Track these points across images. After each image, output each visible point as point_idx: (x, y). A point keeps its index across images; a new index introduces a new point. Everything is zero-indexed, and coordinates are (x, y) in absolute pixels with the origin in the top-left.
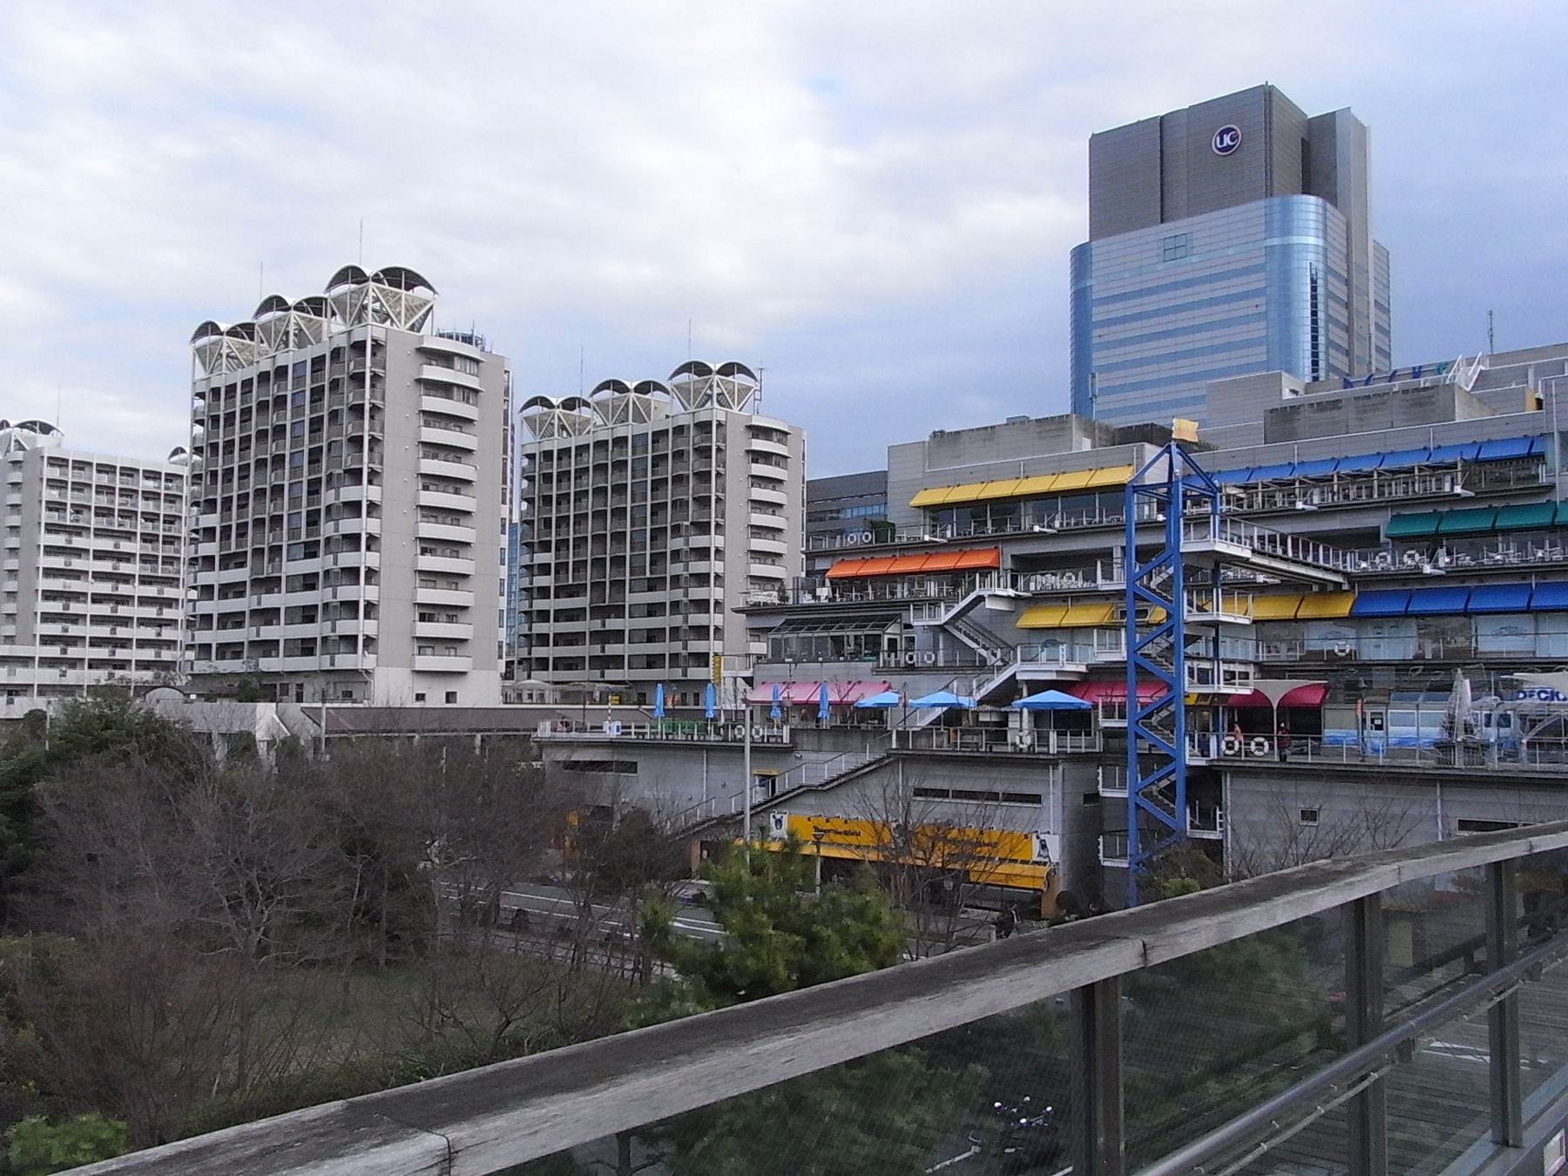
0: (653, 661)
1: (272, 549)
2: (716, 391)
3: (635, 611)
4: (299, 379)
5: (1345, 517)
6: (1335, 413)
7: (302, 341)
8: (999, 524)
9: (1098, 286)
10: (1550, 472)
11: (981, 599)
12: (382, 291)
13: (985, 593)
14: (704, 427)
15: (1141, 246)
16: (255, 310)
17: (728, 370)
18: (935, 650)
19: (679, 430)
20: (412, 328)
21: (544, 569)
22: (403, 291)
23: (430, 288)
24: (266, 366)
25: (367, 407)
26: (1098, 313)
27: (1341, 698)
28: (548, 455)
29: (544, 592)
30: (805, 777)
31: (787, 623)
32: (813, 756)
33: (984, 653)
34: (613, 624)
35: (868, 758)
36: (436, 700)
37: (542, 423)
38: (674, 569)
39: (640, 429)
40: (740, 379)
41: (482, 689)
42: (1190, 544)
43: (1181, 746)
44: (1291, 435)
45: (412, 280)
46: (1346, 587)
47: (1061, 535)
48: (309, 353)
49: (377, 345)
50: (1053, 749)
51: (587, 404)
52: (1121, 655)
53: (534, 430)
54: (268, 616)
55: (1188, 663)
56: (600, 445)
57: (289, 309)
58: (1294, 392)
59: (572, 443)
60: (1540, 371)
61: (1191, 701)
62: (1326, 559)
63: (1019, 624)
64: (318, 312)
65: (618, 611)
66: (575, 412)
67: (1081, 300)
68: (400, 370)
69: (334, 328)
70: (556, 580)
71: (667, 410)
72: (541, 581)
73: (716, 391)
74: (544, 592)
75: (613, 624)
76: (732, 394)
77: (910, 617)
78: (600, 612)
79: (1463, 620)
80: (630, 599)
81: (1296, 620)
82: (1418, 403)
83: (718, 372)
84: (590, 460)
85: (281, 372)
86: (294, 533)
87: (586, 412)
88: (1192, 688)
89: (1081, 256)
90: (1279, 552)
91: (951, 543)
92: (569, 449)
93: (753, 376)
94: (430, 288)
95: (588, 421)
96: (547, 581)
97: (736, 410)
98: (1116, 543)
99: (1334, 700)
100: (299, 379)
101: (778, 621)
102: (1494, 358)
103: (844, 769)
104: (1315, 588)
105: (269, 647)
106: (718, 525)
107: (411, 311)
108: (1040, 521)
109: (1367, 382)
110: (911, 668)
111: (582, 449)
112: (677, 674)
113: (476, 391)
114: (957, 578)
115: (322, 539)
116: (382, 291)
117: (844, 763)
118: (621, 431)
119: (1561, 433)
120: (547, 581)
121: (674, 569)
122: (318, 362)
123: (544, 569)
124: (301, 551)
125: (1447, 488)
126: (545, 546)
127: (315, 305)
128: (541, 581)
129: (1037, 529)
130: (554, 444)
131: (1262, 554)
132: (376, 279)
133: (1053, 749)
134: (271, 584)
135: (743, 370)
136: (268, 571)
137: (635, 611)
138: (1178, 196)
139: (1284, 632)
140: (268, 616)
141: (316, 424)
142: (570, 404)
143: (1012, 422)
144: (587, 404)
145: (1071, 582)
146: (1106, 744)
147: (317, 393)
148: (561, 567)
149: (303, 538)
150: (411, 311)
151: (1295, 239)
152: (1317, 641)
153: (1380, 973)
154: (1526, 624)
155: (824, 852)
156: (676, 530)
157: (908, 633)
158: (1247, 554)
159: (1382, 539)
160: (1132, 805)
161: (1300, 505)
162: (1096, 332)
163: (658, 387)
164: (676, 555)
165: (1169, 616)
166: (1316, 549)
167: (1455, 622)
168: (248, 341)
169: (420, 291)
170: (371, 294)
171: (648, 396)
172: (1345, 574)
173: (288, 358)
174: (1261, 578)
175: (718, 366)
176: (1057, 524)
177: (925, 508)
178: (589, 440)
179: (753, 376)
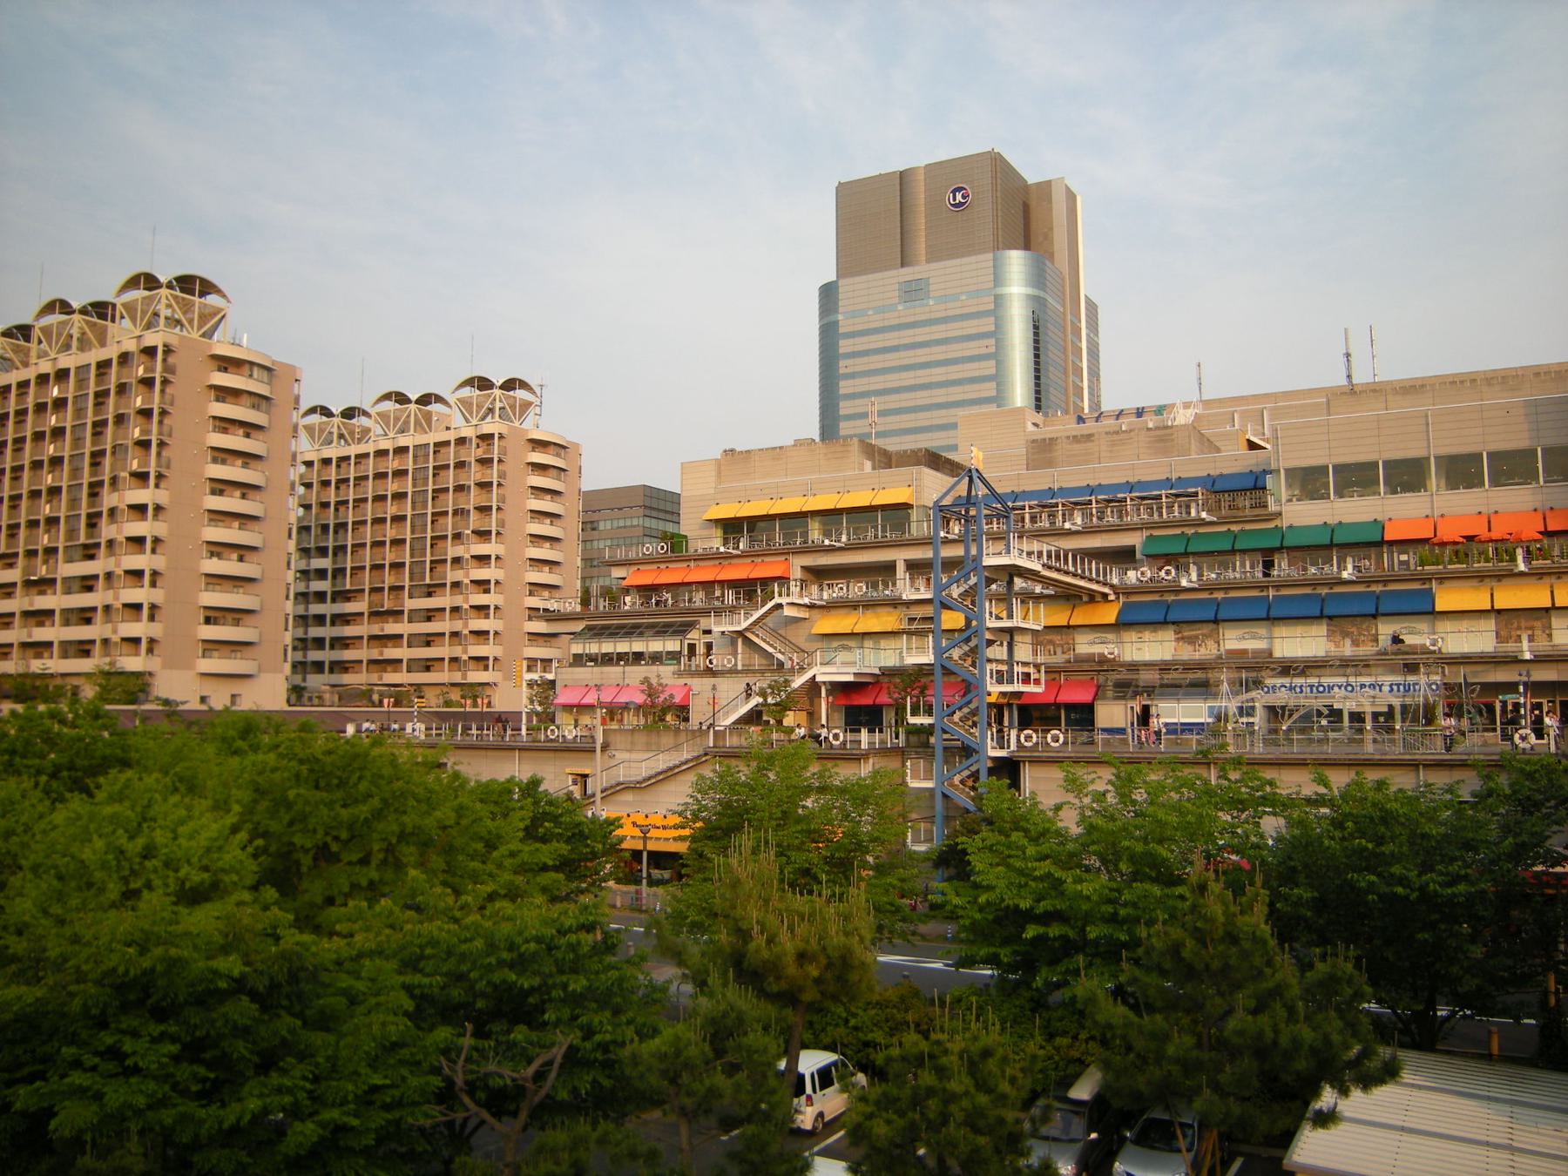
0: (428, 665)
1: (392, 588)
2: (498, 405)
3: (414, 616)
4: (82, 382)
5: (1104, 536)
6: (1089, 445)
7: (84, 345)
8: (789, 536)
9: (845, 323)
10: (1278, 501)
11: (780, 606)
12: (175, 297)
13: (784, 600)
14: (486, 438)
15: (877, 293)
16: (37, 309)
17: (510, 385)
18: (735, 654)
19: (461, 441)
20: (203, 335)
21: (321, 574)
22: (196, 299)
23: (224, 296)
24: (46, 367)
25: (156, 412)
26: (845, 346)
27: (1110, 694)
28: (326, 462)
29: (320, 597)
30: (622, 774)
31: (589, 628)
32: (626, 756)
33: (780, 657)
34: (391, 628)
35: (686, 756)
36: (219, 701)
37: (321, 431)
38: (452, 575)
39: (421, 439)
40: (520, 394)
41: (268, 693)
42: (993, 558)
43: (984, 737)
44: (1050, 464)
45: (207, 288)
46: (1112, 597)
47: (848, 548)
48: (94, 356)
49: (168, 350)
50: (864, 746)
51: (366, 414)
52: (928, 658)
53: (312, 437)
54: (41, 617)
55: (989, 667)
56: (381, 453)
57: (73, 312)
58: (1035, 425)
59: (353, 450)
60: (1243, 414)
61: (992, 699)
62: (1105, 574)
63: (814, 631)
64: (103, 316)
65: (396, 614)
66: (354, 421)
67: (829, 335)
68: (193, 377)
69: (124, 336)
70: (334, 585)
71: (455, 422)
72: (318, 586)
73: (498, 405)
74: (320, 597)
75: (391, 628)
76: (513, 407)
77: (704, 623)
78: (377, 615)
79: (1212, 626)
80: (410, 604)
81: (1068, 627)
82: (1161, 440)
83: (502, 387)
84: (370, 467)
85: (62, 375)
86: (72, 533)
87: (364, 421)
88: (995, 689)
89: (828, 294)
90: (1071, 569)
91: (743, 556)
92: (348, 458)
93: (534, 393)
94: (224, 296)
95: (369, 430)
96: (324, 586)
97: (517, 424)
98: (900, 556)
99: (1104, 698)
100: (82, 382)
101: (578, 626)
102: (1207, 404)
103: (662, 766)
104: (1085, 599)
105: (41, 648)
106: (498, 533)
107: (204, 318)
108: (827, 534)
109: (1097, 419)
110: (710, 672)
111: (362, 457)
112: (457, 677)
113: (267, 398)
114: (750, 590)
115: (103, 542)
116: (175, 297)
117: (663, 762)
118: (403, 441)
119: (1286, 470)
120: (324, 586)
121: (452, 575)
122: (103, 366)
123: (321, 574)
124: (80, 552)
125: (1193, 513)
126: (322, 552)
127: (101, 310)
128: (318, 586)
129: (827, 542)
130: (333, 452)
131: (1050, 568)
132: (170, 286)
133: (864, 746)
134: (45, 584)
135: (524, 385)
136: (43, 571)
137: (414, 616)
138: (920, 245)
139: (1057, 638)
140: (41, 617)
141: (99, 426)
142: (349, 413)
143: (798, 443)
144: (366, 414)
145: (858, 589)
146: (907, 740)
147: (101, 396)
148: (339, 572)
149: (82, 540)
150: (204, 318)
151: (1030, 291)
152: (1085, 645)
153: (573, 845)
154: (1262, 630)
155: (652, 846)
156: (457, 536)
157: (708, 639)
158: (1038, 567)
159: (1138, 556)
160: (939, 797)
161: (1067, 525)
162: (841, 363)
163: (439, 399)
164: (457, 561)
165: (968, 622)
166: (1083, 563)
167: (1206, 629)
168: (22, 343)
169: (212, 300)
170: (164, 301)
171: (429, 408)
172: (1112, 586)
173: (68, 361)
174: (1038, 589)
175: (501, 382)
176: (844, 538)
177: (717, 521)
178: (369, 448)
179: (534, 393)
